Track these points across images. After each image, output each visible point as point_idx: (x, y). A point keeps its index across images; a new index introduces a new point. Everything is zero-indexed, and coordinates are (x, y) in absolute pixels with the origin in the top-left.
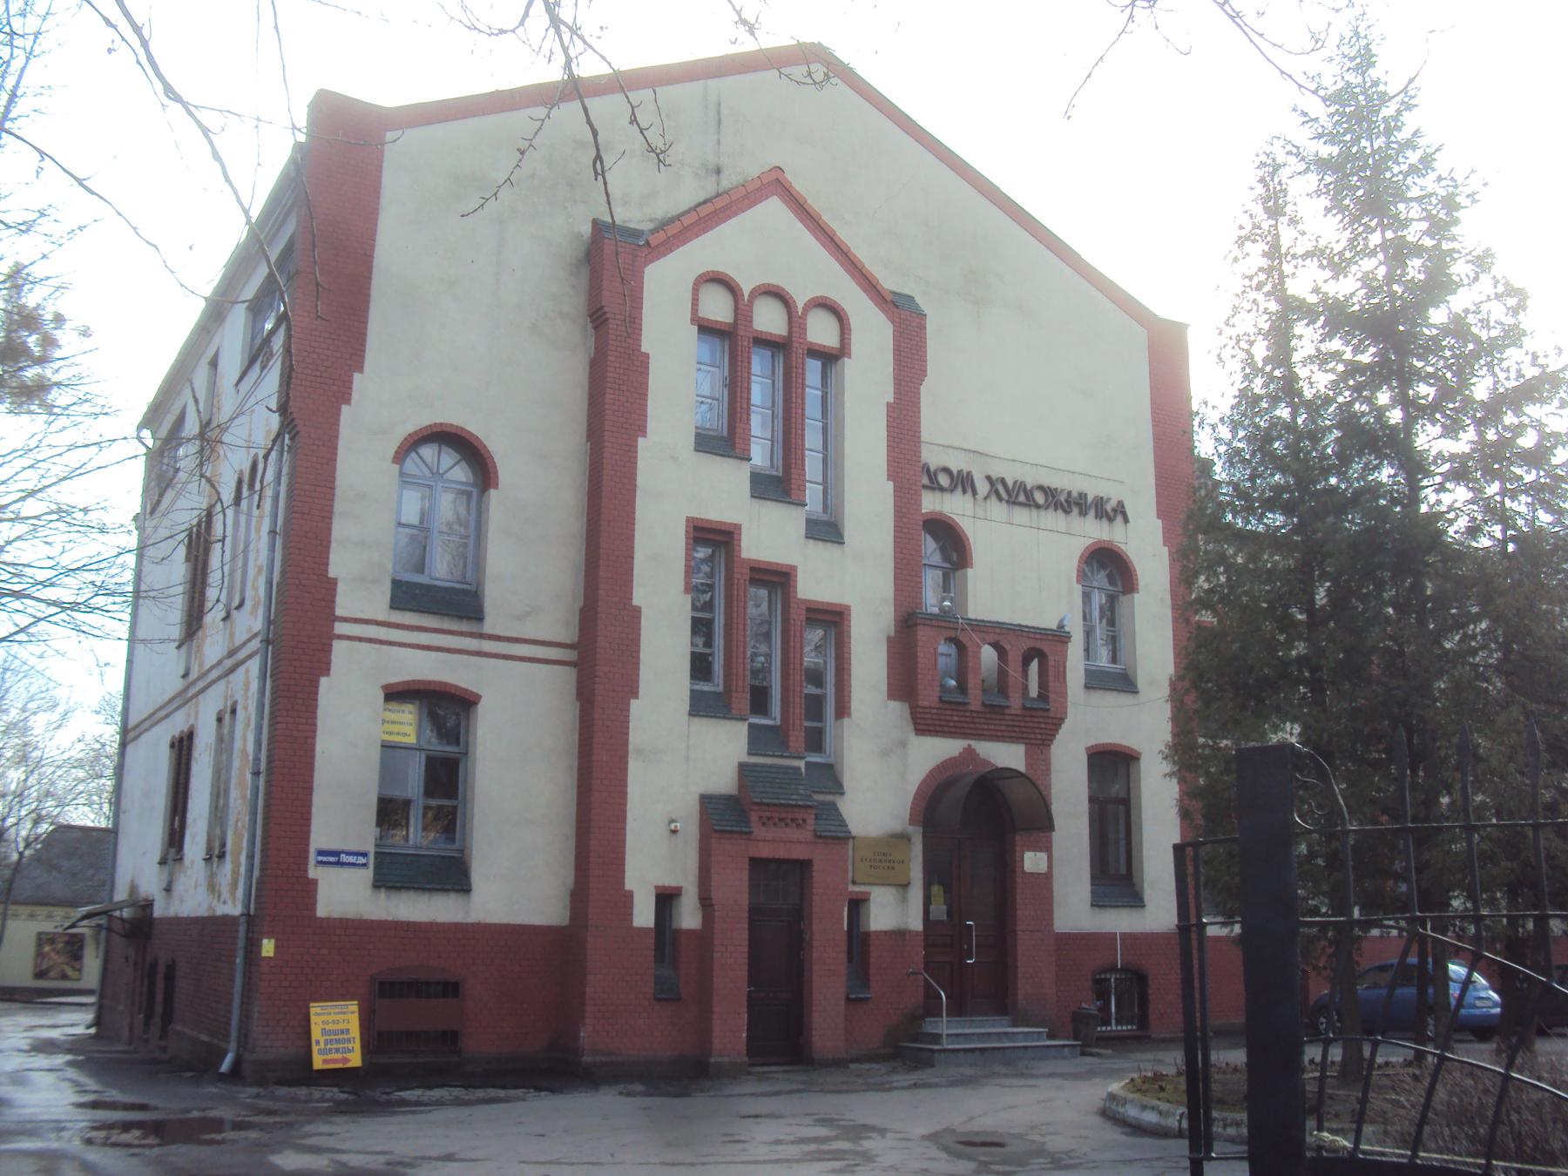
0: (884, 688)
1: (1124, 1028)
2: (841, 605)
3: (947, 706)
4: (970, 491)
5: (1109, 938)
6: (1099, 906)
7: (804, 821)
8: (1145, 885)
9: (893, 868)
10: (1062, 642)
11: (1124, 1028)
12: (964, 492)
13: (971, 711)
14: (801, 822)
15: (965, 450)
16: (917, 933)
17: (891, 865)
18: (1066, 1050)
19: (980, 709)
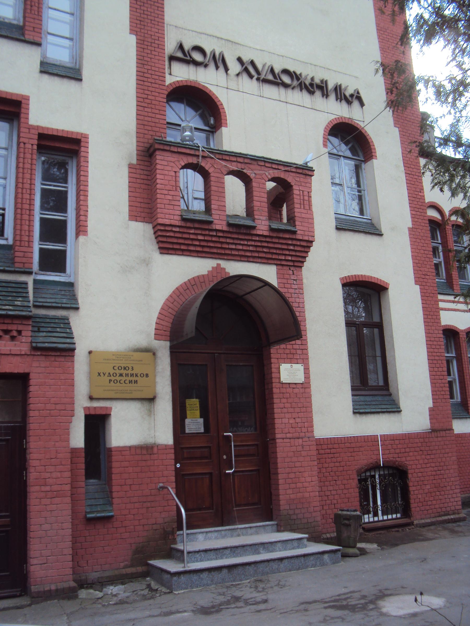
0: (125, 209)
1: (390, 517)
2: (78, 133)
3: (189, 224)
4: (222, 68)
5: (371, 440)
6: (360, 413)
7: (19, 332)
8: (400, 393)
9: (136, 382)
10: (306, 175)
11: (390, 517)
12: (217, 68)
13: (217, 231)
14: (15, 334)
15: (218, 38)
16: (166, 447)
17: (134, 378)
18: (326, 556)
19: (225, 228)
